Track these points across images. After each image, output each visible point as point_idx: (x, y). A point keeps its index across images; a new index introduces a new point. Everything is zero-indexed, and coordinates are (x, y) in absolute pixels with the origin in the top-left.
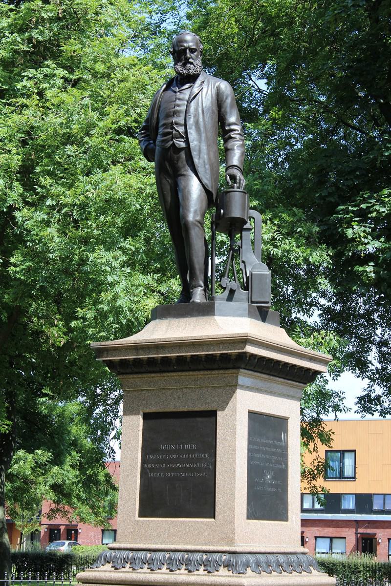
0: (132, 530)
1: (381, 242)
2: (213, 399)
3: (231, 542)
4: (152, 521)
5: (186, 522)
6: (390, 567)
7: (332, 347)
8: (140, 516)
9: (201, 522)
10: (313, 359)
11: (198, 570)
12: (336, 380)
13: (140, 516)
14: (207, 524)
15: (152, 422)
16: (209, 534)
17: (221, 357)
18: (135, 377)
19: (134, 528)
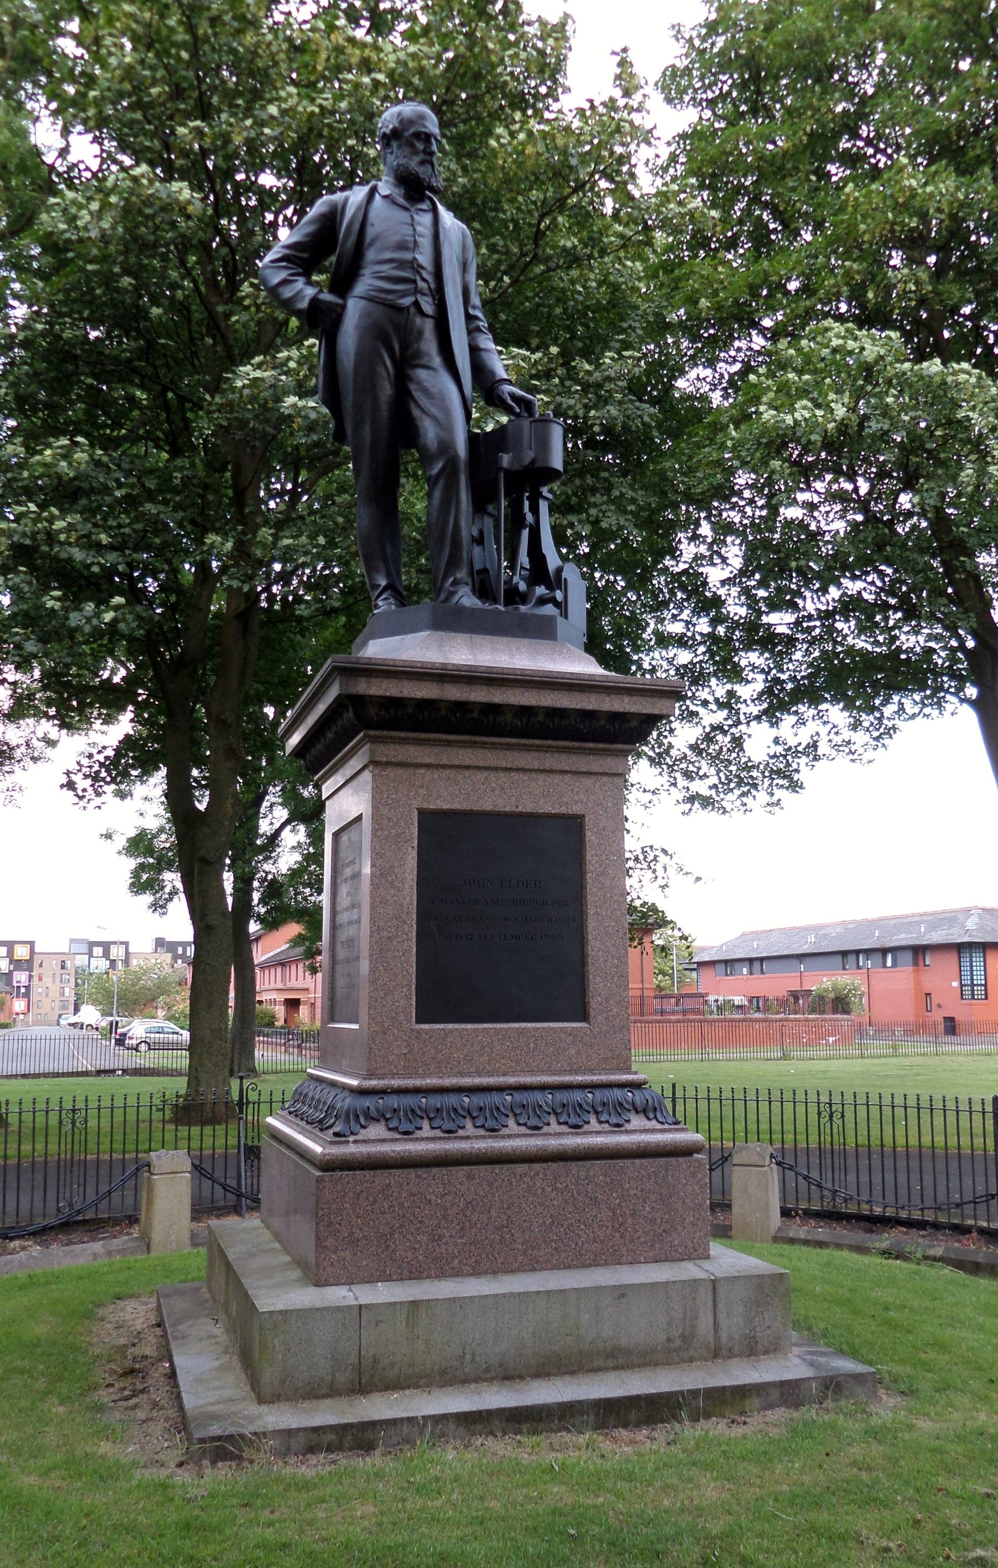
0: (405, 1051)
1: (722, 34)
2: (576, 797)
3: (628, 1070)
4: (451, 1031)
5: (528, 1030)
6: (992, 1438)
7: (15, 160)
8: (418, 1022)
9: (562, 1029)
10: (296, 1443)
11: (421, 1129)
12: (49, 752)
13: (418, 1022)
14: (572, 1033)
15: (336, 1017)
16: (578, 1052)
17: (487, 307)
18: (257, 1338)
19: (408, 1045)
